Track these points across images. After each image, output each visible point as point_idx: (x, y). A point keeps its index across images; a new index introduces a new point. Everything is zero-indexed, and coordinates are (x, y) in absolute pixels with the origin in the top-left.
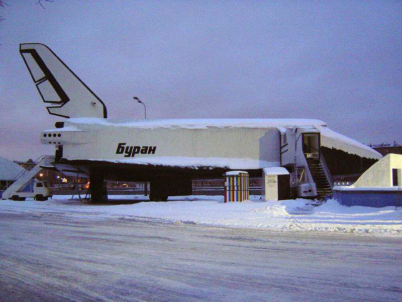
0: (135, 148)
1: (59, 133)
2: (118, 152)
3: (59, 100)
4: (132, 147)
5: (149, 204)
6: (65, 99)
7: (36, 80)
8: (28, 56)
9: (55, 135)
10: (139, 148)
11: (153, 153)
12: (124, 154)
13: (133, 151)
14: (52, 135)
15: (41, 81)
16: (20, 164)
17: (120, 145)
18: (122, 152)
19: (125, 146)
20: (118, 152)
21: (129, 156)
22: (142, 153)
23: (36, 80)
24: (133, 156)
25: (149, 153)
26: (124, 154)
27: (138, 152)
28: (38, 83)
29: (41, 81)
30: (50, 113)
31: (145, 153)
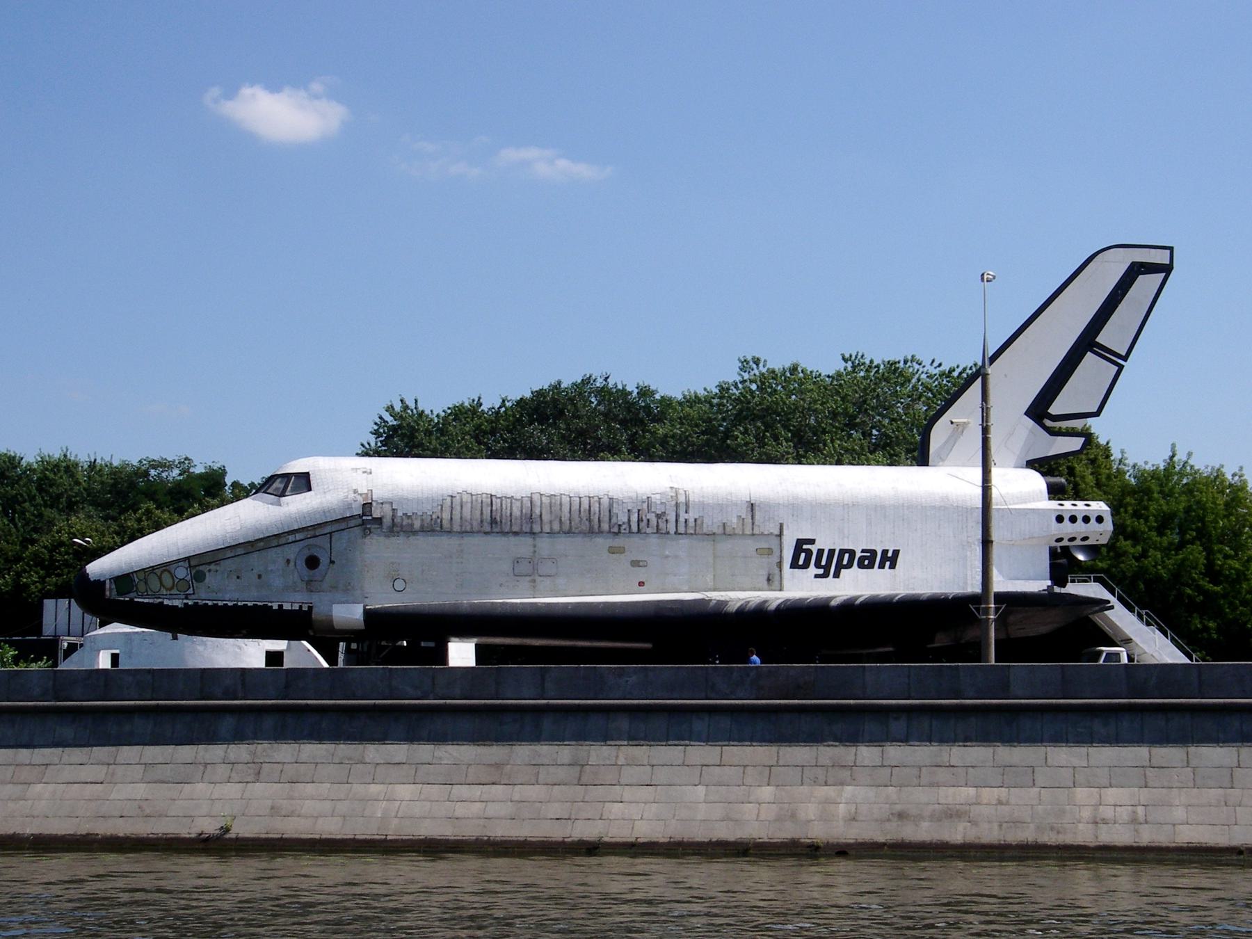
4: (832, 552)
7: (1116, 368)
9: (1073, 519)
10: (852, 553)
11: (893, 566)
12: (813, 570)
13: (834, 562)
15: (1106, 353)
18: (806, 565)
19: (814, 549)
21: (825, 575)
22: (861, 566)
23: (1116, 368)
24: (837, 575)
25: (882, 566)
26: (813, 570)
27: (849, 566)
28: (1117, 360)
29: (1106, 353)
31: (871, 566)
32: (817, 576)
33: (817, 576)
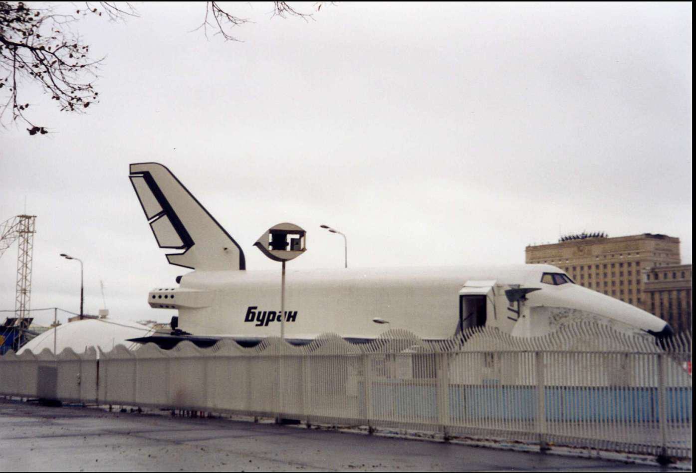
0: (270, 313)
1: (151, 297)
2: (247, 320)
3: (181, 244)
5: (302, 256)
6: (188, 243)
7: (150, 217)
8: (141, 182)
11: (294, 320)
12: (256, 322)
13: (266, 318)
14: (169, 296)
16: (203, 308)
17: (250, 308)
18: (252, 320)
19: (257, 311)
20: (247, 320)
21: (261, 325)
24: (267, 325)
26: (256, 322)
27: (273, 320)
28: (152, 220)
30: (170, 263)
32: (257, 325)
33: (257, 325)
